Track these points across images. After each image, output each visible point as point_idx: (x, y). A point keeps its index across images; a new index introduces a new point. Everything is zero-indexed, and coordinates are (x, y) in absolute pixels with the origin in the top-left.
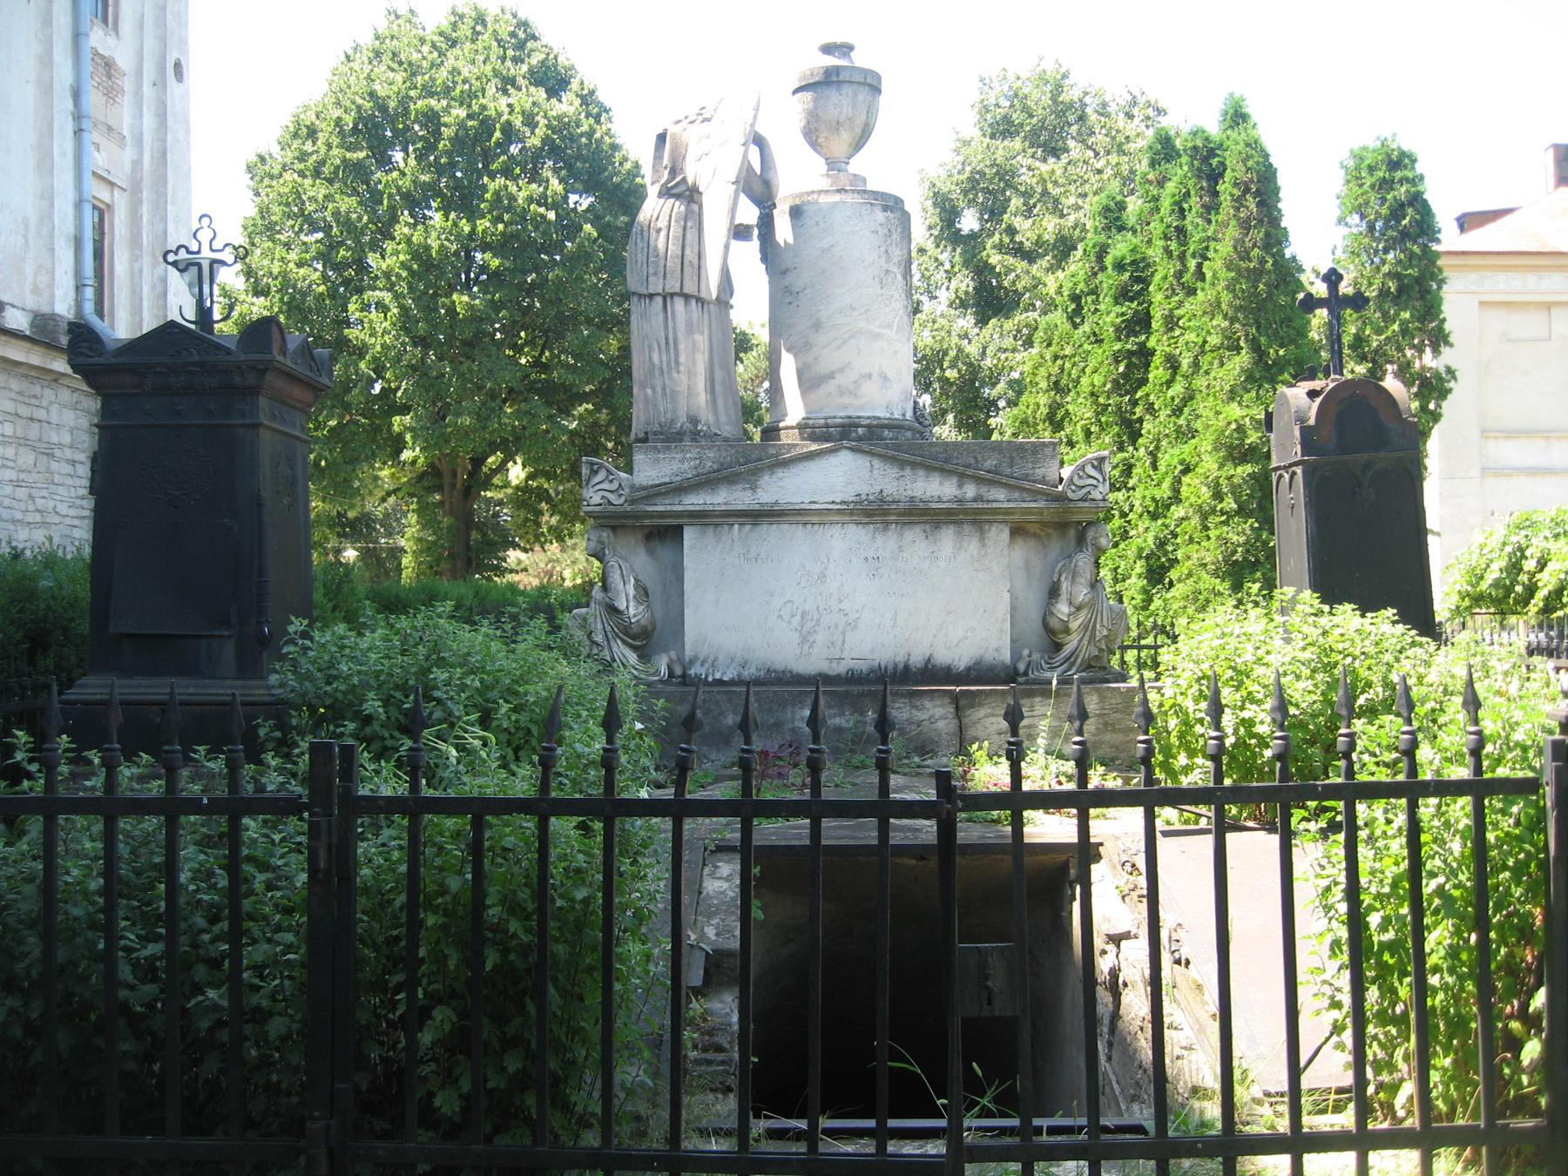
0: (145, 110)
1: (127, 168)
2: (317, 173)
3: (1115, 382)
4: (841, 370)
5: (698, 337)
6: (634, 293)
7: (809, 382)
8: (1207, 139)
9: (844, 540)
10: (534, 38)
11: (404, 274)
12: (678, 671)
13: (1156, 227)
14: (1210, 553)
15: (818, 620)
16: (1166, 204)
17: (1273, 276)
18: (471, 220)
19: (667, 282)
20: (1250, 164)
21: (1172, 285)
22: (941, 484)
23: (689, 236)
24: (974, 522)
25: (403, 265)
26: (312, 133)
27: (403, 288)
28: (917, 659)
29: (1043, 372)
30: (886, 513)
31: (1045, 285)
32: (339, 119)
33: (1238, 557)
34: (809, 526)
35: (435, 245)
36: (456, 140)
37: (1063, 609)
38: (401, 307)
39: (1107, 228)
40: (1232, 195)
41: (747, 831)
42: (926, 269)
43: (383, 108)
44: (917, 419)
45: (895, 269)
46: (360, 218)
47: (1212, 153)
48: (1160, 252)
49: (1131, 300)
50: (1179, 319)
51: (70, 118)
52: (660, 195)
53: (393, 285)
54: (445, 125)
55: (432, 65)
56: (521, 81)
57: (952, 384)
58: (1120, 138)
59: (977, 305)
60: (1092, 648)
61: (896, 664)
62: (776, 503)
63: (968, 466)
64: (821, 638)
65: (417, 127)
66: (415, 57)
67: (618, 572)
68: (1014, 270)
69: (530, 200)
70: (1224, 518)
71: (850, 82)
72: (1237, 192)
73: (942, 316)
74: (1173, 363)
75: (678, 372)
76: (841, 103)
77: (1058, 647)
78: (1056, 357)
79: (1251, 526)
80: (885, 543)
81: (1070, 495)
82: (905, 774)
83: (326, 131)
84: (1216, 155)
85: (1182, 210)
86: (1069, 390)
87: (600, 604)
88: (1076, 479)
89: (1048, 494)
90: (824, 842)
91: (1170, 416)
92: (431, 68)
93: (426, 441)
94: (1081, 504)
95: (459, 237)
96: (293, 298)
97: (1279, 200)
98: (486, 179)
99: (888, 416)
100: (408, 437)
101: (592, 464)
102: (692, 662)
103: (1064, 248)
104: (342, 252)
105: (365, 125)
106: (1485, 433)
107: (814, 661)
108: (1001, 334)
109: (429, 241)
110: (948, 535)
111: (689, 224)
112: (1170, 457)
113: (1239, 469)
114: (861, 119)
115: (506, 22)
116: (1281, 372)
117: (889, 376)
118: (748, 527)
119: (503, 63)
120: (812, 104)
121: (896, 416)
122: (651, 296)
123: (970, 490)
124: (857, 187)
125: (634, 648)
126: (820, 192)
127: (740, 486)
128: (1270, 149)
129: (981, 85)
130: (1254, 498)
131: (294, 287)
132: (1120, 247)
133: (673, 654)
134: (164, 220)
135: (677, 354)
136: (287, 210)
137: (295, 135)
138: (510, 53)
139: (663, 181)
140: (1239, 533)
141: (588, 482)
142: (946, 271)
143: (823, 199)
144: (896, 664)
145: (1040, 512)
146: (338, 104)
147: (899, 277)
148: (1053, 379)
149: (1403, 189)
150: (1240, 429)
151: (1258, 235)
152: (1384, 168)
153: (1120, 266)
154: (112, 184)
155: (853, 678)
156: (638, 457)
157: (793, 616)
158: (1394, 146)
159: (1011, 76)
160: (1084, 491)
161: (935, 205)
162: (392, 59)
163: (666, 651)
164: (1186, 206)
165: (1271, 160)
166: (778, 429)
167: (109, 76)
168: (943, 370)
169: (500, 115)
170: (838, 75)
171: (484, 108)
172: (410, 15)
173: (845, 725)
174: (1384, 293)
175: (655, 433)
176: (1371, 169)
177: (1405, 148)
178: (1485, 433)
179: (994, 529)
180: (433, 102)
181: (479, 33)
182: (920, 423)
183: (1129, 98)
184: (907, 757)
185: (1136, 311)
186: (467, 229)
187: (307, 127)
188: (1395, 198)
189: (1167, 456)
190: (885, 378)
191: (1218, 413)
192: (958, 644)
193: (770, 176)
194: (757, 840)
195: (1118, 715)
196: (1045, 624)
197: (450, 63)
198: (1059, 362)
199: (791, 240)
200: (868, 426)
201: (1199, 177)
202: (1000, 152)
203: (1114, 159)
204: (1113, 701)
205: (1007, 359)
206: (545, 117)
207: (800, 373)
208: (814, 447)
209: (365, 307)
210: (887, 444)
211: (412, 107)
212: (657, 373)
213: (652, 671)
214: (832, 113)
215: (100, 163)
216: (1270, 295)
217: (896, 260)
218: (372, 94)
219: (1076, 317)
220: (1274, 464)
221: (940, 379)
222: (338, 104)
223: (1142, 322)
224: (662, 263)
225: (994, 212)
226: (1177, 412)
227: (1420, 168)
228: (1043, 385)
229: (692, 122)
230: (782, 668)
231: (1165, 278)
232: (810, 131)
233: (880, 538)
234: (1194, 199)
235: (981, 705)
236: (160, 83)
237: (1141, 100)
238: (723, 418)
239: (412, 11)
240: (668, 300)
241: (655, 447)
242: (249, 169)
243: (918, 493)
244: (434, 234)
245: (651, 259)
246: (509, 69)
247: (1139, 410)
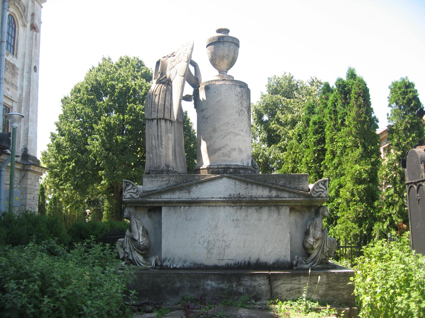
0: (24, 80)
1: (18, 96)
2: (80, 102)
3: (314, 159)
4: (224, 147)
5: (170, 135)
6: (147, 119)
7: (211, 152)
8: (343, 82)
10: (143, 65)
11: (103, 130)
12: (159, 264)
13: (326, 111)
14: (351, 214)
15: (214, 244)
16: (329, 103)
17: (369, 123)
18: (123, 115)
20: (360, 87)
21: (332, 128)
22: (263, 191)
23: (167, 98)
24: (275, 206)
25: (103, 128)
26: (79, 91)
27: (103, 134)
28: (253, 260)
29: (290, 157)
30: (241, 202)
31: (289, 133)
32: (87, 87)
33: (360, 216)
34: (211, 207)
35: (112, 122)
36: (119, 93)
37: (311, 240)
38: (102, 140)
39: (309, 113)
40: (355, 97)
42: (253, 131)
43: (99, 84)
44: (253, 166)
45: (244, 109)
46: (92, 115)
47: (345, 86)
48: (328, 118)
49: (319, 134)
50: (335, 139)
52: (157, 83)
53: (100, 133)
54: (117, 89)
55: (114, 72)
56: (139, 77)
57: (261, 163)
58: (310, 91)
59: (268, 141)
60: (323, 256)
61: (245, 262)
62: (198, 198)
63: (273, 184)
64: (215, 251)
65: (109, 89)
66: (109, 70)
67: (136, 225)
68: (280, 129)
69: (140, 110)
70: (355, 203)
71: (228, 42)
72: (356, 96)
73: (258, 144)
74: (333, 153)
75: (162, 148)
76: (224, 49)
77: (309, 255)
78: (294, 153)
79: (365, 206)
80: (241, 214)
81: (313, 195)
82: (249, 308)
83: (83, 90)
84: (346, 87)
85: (335, 105)
86: (298, 163)
87: (128, 237)
88: (315, 189)
89: (304, 195)
91: (333, 170)
92: (113, 73)
93: (108, 178)
94: (317, 199)
95: (119, 120)
96: (72, 137)
97: (370, 99)
98: (127, 104)
99: (242, 164)
100: (103, 177)
101: (127, 182)
102: (165, 260)
103: (294, 123)
104: (86, 124)
105: (94, 89)
107: (212, 261)
108: (275, 149)
109: (111, 121)
110: (265, 211)
111: (167, 93)
112: (334, 183)
113: (360, 186)
114: (232, 55)
115: (135, 61)
116: (373, 154)
117: (242, 149)
118: (187, 207)
119: (134, 72)
120: (213, 50)
121: (245, 165)
122: (152, 120)
123: (274, 193)
124: (231, 79)
125: (142, 255)
126: (216, 80)
127: (184, 191)
128: (367, 83)
129: (268, 80)
130: (365, 196)
131: (72, 134)
132: (314, 118)
133: (157, 257)
134: (29, 111)
136: (71, 112)
137: (75, 92)
138: (136, 69)
139: (158, 78)
140: (360, 208)
141: (125, 189)
142: (259, 132)
143: (217, 83)
144: (245, 262)
145: (301, 201)
146: (87, 83)
148: (293, 159)
149: (411, 94)
150: (360, 173)
151: (364, 110)
152: (404, 88)
153: (315, 123)
154: (13, 101)
155: (228, 267)
156: (145, 180)
157: (204, 242)
158: (407, 81)
159: (277, 77)
160: (319, 193)
161: (256, 113)
162: (103, 72)
163: (155, 256)
164: (336, 104)
165: (367, 86)
166: (200, 170)
167: (14, 69)
168: (258, 159)
169: (132, 86)
170: (223, 39)
171: (128, 84)
172: (109, 59)
173: (224, 287)
174: (406, 129)
175: (153, 171)
176: (400, 88)
177: (410, 81)
179: (283, 208)
180: (113, 82)
181: (128, 64)
182: (254, 168)
183: (312, 80)
184: (249, 301)
185: (320, 137)
186: (122, 118)
187: (78, 89)
188: (408, 97)
189: (333, 183)
190: (240, 150)
191: (352, 168)
192: (269, 254)
193: (198, 77)
195: (335, 283)
196: (304, 246)
197: (119, 72)
198: (295, 154)
199: (205, 98)
200: (234, 168)
201: (341, 94)
202: (274, 98)
203: (308, 97)
204: (332, 278)
205: (277, 155)
206: (145, 87)
207: (208, 148)
208: (213, 176)
209: (93, 140)
210: (241, 175)
211: (107, 83)
212: (154, 148)
213: (149, 264)
214: (221, 53)
215: (9, 94)
216: (368, 129)
217: (245, 106)
218: (96, 80)
219: (300, 140)
220: (407, 182)
221: (257, 162)
222: (87, 83)
223: (322, 141)
224: (157, 107)
225: (273, 115)
226: (336, 168)
227: (416, 88)
228: (290, 161)
229: (169, 57)
230: (200, 263)
231: (330, 126)
232: (213, 59)
233: (239, 212)
234: (339, 101)
235: (279, 279)
236: (29, 72)
237: (316, 81)
238: (179, 166)
239: (109, 58)
240: (159, 121)
241: (152, 176)
242: (62, 101)
243: (254, 195)
244: (112, 119)
245: (153, 106)
246: (135, 74)
247: (322, 168)
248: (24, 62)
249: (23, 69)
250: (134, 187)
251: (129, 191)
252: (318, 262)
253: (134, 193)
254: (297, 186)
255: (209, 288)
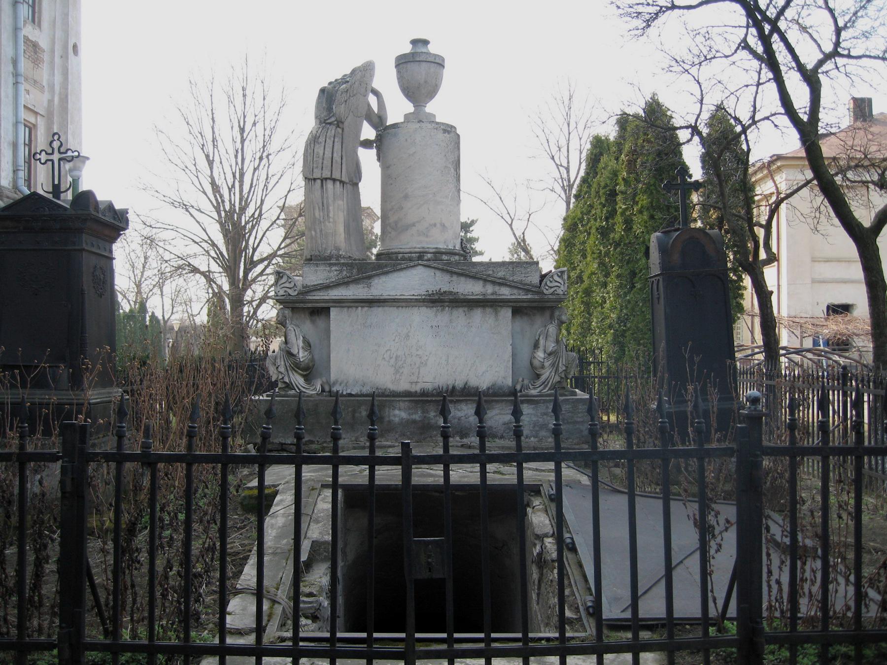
0: (56, 72)
1: (45, 104)
4: (419, 222)
9: (420, 316)
12: (327, 388)
15: (405, 361)
19: (324, 171)
28: (459, 384)
37: (540, 354)
41: (335, 475)
45: (450, 166)
51: (11, 75)
67: (294, 333)
76: (420, 72)
77: (538, 376)
81: (545, 291)
90: (377, 483)
102: (334, 384)
106: (814, 260)
107: (403, 386)
110: (478, 313)
111: (336, 140)
117: (446, 225)
121: (450, 247)
122: (315, 179)
123: (490, 289)
133: (324, 380)
135: (328, 212)
147: (452, 170)
154: (36, 113)
155: (424, 393)
160: (553, 290)
167: (36, 53)
178: (814, 260)
182: (464, 251)
190: (443, 226)
194: (341, 480)
196: (531, 364)
217: (451, 161)
240: (324, 181)
248: (54, 36)
249: (53, 51)
250: (290, 280)
251: (282, 286)
252: (551, 386)
253: (290, 288)
254: (524, 279)
255: (397, 420)
